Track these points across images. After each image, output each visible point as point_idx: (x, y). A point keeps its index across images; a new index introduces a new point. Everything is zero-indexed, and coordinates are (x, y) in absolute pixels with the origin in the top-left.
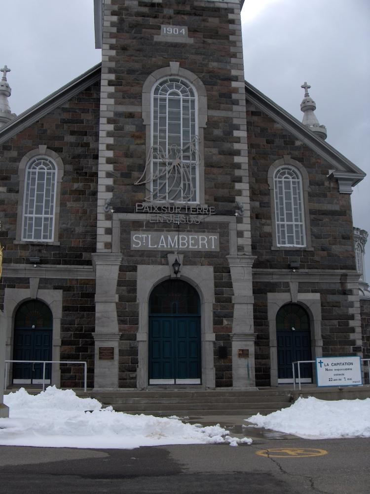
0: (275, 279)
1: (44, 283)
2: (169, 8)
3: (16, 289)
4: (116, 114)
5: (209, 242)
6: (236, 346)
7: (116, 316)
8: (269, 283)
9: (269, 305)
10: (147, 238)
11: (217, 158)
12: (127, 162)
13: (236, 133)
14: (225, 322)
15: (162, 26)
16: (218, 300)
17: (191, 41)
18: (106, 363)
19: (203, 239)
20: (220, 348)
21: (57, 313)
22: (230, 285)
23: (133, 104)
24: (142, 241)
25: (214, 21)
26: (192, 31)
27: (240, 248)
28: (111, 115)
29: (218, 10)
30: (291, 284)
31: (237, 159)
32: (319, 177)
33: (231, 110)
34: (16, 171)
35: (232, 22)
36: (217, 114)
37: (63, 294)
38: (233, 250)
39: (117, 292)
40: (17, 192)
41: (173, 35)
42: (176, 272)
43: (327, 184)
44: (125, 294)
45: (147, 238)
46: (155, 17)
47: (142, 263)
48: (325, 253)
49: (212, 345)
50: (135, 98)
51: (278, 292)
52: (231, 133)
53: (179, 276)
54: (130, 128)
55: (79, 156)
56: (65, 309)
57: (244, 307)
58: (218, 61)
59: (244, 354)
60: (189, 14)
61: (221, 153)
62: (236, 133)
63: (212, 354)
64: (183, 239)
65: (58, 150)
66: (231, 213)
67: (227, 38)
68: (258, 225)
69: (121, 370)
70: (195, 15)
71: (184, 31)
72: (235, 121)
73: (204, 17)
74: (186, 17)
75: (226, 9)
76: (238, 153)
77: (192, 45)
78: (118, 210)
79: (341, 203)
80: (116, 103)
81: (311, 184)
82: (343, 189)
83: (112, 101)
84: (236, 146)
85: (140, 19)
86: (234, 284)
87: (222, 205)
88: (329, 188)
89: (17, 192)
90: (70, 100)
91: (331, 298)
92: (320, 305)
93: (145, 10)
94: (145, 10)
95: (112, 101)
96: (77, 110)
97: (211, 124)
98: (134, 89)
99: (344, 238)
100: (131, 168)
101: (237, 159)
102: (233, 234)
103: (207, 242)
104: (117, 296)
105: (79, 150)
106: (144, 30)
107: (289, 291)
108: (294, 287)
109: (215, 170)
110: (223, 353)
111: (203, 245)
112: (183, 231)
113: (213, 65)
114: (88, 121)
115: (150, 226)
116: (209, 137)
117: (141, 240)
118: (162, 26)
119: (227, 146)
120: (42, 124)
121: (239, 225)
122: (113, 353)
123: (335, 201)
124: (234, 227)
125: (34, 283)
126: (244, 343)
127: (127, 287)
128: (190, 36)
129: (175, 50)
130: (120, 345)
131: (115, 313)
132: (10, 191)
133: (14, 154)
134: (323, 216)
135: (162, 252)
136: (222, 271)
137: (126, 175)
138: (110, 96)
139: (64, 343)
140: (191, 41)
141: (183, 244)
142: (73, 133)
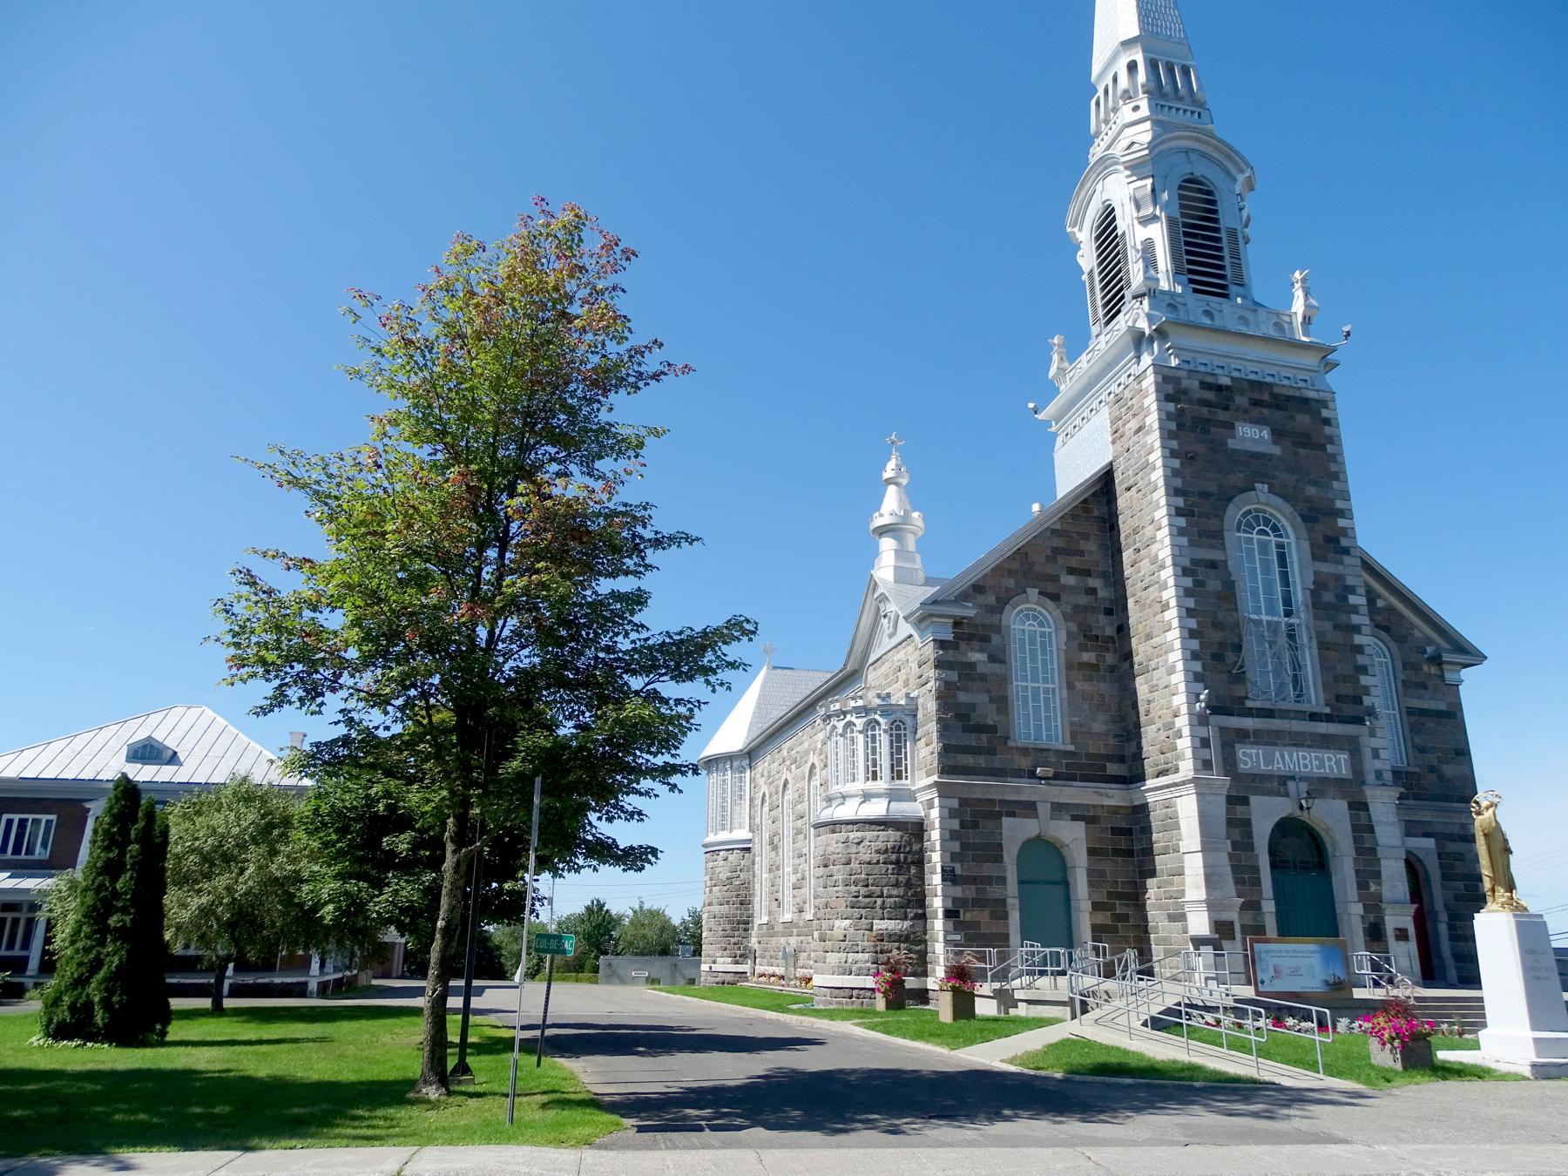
1: (1058, 809)
4: (1194, 562)
5: (1338, 763)
11: (1333, 636)
13: (1353, 600)
14: (1373, 888)
17: (1276, 450)
19: (1330, 759)
22: (1371, 829)
23: (1213, 547)
25: (1303, 420)
26: (1278, 435)
32: (1414, 658)
34: (998, 629)
35: (1327, 422)
36: (1325, 568)
38: (1370, 777)
41: (1254, 440)
43: (1425, 668)
46: (1226, 408)
49: (1359, 921)
50: (1214, 537)
52: (1345, 599)
53: (1305, 817)
54: (1214, 585)
55: (1086, 608)
56: (1092, 852)
57: (1393, 863)
58: (1315, 483)
60: (1269, 406)
61: (1337, 627)
62: (1353, 600)
63: (1361, 935)
64: (1304, 758)
65: (1055, 597)
66: (1360, 721)
67: (1323, 448)
70: (1278, 408)
71: (1266, 434)
72: (1350, 581)
74: (1266, 411)
80: (1192, 543)
84: (1355, 619)
85: (1205, 410)
86: (1377, 829)
87: (1348, 710)
91: (1453, 847)
93: (1210, 395)
94: (1210, 395)
102: (1367, 753)
103: (1334, 763)
105: (1084, 600)
109: (1331, 654)
113: (1311, 491)
115: (1259, 738)
117: (1251, 758)
119: (1342, 618)
124: (1368, 743)
125: (1044, 810)
128: (1275, 443)
131: (1229, 869)
132: (993, 659)
135: (1279, 777)
136: (1359, 807)
139: (1097, 907)
140: (1276, 450)
141: (1306, 766)
142: (1071, 571)
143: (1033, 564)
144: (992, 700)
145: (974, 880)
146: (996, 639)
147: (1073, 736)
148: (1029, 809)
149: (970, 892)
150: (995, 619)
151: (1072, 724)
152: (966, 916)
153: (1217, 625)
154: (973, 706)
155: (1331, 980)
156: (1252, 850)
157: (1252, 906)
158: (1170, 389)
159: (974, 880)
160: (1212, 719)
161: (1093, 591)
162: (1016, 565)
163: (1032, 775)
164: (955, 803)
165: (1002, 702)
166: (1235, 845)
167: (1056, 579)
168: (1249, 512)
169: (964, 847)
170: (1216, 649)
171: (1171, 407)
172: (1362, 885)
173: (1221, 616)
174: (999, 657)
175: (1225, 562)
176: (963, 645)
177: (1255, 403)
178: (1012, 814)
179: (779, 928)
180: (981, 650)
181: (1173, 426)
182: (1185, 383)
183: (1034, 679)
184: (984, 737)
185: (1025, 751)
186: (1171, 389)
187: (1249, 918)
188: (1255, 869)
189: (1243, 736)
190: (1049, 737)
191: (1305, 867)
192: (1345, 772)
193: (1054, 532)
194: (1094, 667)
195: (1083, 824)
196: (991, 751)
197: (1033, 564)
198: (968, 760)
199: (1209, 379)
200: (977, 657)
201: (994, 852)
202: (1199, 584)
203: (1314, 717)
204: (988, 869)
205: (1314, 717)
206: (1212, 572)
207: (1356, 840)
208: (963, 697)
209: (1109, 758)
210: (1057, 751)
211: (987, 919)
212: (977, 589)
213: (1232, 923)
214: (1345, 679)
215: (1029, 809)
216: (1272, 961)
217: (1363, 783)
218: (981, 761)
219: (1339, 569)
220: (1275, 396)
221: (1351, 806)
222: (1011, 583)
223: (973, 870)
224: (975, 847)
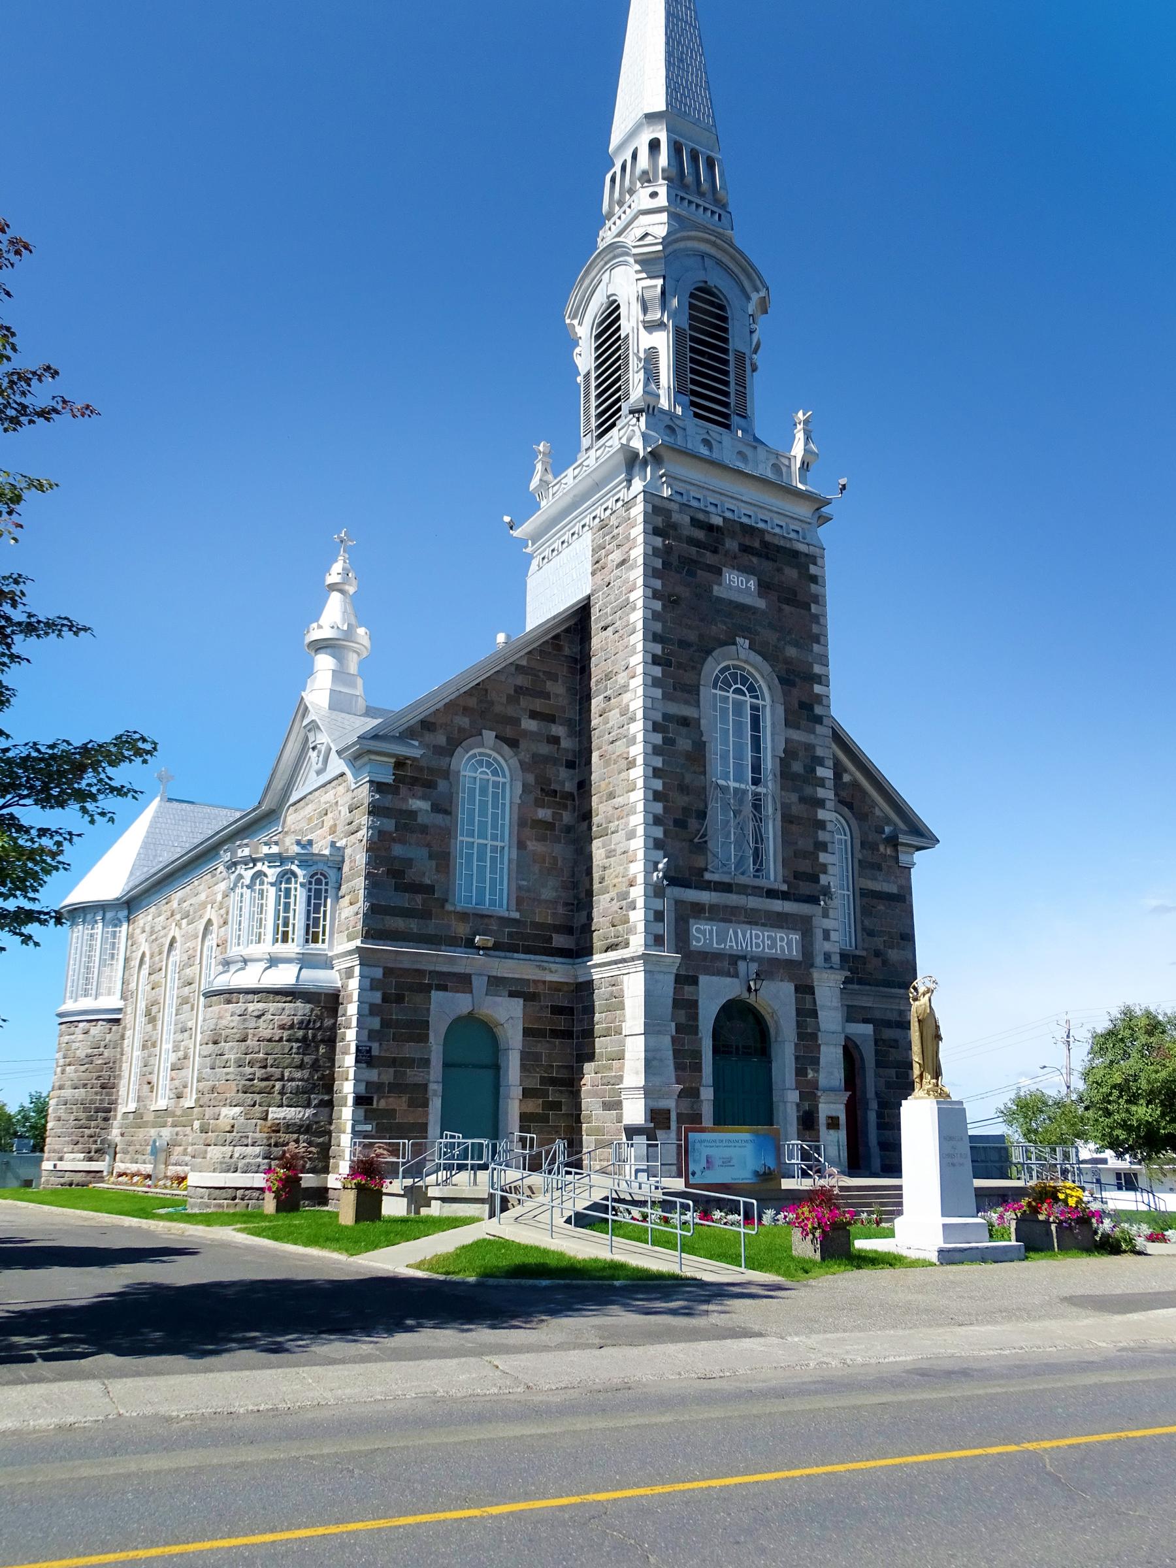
4: (666, 716)
5: (789, 944)
7: (671, 1057)
10: (711, 932)
11: (797, 809)
12: (682, 800)
14: (811, 1075)
17: (761, 604)
20: (805, 1112)
21: (513, 1038)
23: (687, 702)
24: (705, 936)
25: (791, 573)
26: (764, 587)
27: (827, 957)
29: (796, 554)
34: (446, 774)
38: (819, 960)
41: (739, 590)
43: (882, 848)
44: (683, 1020)
45: (711, 932)
49: (794, 1107)
50: (689, 692)
52: (814, 771)
56: (527, 1032)
57: (832, 1049)
58: (796, 644)
59: (833, 1123)
60: (757, 554)
64: (757, 937)
65: (513, 743)
66: (813, 900)
71: (752, 584)
72: (820, 752)
75: (807, 555)
80: (666, 697)
82: (903, 858)
87: (805, 888)
90: (529, 653)
91: (888, 1033)
92: (873, 1043)
93: (700, 535)
94: (700, 535)
96: (541, 674)
97: (790, 753)
98: (688, 677)
99: (902, 939)
100: (686, 810)
102: (819, 934)
103: (786, 944)
104: (673, 1024)
105: (545, 749)
106: (699, 572)
111: (782, 947)
112: (756, 924)
113: (791, 652)
114: (557, 695)
117: (704, 934)
119: (808, 790)
121: (825, 920)
122: (669, 1119)
125: (479, 984)
126: (832, 1106)
128: (760, 595)
130: (677, 1106)
132: (437, 808)
134: (875, 901)
135: (731, 956)
136: (805, 990)
140: (761, 604)
142: (534, 715)
143: (492, 703)
144: (431, 857)
145: (393, 1062)
146: (442, 785)
147: (519, 901)
148: (463, 982)
149: (388, 1076)
151: (519, 888)
153: (683, 789)
154: (409, 862)
155: (761, 1170)
156: (697, 1034)
158: (659, 521)
159: (393, 1062)
160: (669, 891)
161: (555, 740)
162: (472, 702)
163: (470, 944)
164: (378, 973)
165: (443, 859)
166: (679, 1028)
167: (516, 722)
169: (385, 1024)
172: (800, 1072)
173: (688, 778)
174: (444, 808)
176: (403, 790)
177: (745, 549)
178: (444, 988)
179: (149, 1117)
180: (424, 798)
181: (658, 563)
183: (482, 835)
184: (419, 898)
185: (464, 916)
188: (697, 1054)
189: (698, 910)
190: (492, 902)
192: (795, 953)
193: (519, 668)
194: (550, 826)
195: (521, 1001)
196: (424, 914)
197: (492, 703)
198: (399, 923)
200: (418, 804)
201: (418, 1030)
204: (409, 1050)
206: (684, 730)
207: (799, 1025)
208: (398, 850)
209: (558, 929)
211: (404, 1107)
212: (427, 725)
213: (669, 1111)
215: (463, 982)
217: (812, 965)
218: (413, 925)
220: (766, 544)
221: (797, 989)
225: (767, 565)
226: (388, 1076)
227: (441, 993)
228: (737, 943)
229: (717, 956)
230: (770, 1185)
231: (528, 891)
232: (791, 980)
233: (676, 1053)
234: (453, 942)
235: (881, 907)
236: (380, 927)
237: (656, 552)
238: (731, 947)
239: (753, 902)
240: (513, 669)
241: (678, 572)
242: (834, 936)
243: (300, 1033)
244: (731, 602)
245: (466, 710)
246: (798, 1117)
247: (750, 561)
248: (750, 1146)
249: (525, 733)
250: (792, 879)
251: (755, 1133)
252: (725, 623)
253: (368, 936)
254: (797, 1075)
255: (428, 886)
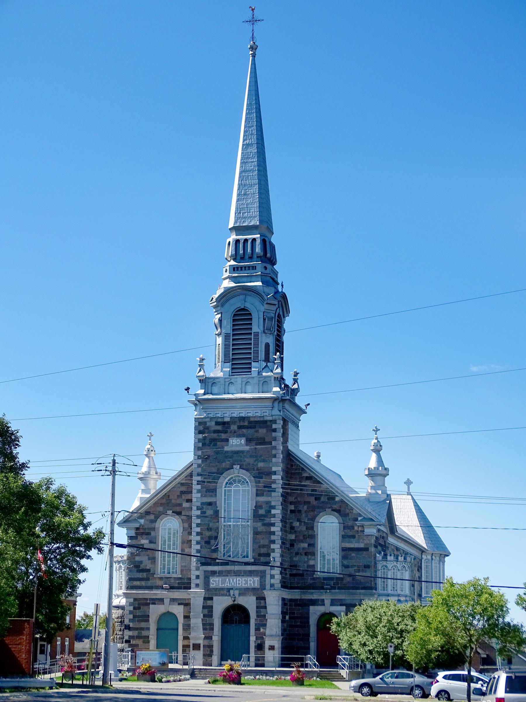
0: (315, 597)
2: (235, 424)
3: (156, 606)
4: (202, 504)
5: (254, 582)
6: (268, 643)
8: (311, 599)
9: (310, 614)
10: (219, 581)
14: (262, 630)
15: (230, 439)
16: (258, 616)
17: (247, 448)
18: (196, 652)
20: (258, 644)
22: (265, 607)
23: (212, 496)
25: (262, 431)
26: (249, 441)
27: (272, 585)
28: (199, 504)
29: (265, 422)
30: (325, 601)
31: (273, 529)
33: (271, 496)
34: (154, 529)
37: (184, 608)
38: (268, 586)
39: (202, 612)
40: (155, 543)
41: (237, 445)
42: (234, 601)
45: (219, 581)
46: (226, 432)
47: (216, 595)
48: (351, 578)
50: (213, 492)
51: (317, 605)
52: (270, 511)
53: (236, 603)
54: (210, 512)
57: (273, 620)
58: (264, 461)
59: (272, 648)
61: (264, 525)
62: (273, 512)
65: (179, 513)
68: (306, 559)
69: (204, 655)
70: (251, 428)
71: (243, 441)
72: (273, 504)
73: (257, 429)
74: (245, 431)
75: (271, 421)
76: (273, 525)
77: (248, 451)
78: (203, 564)
79: (365, 542)
81: (344, 528)
83: (199, 495)
86: (268, 607)
87: (263, 559)
88: (358, 531)
89: (155, 543)
93: (219, 428)
94: (219, 428)
95: (199, 495)
97: (258, 507)
100: (210, 538)
101: (273, 529)
102: (268, 577)
103: (253, 582)
107: (324, 605)
108: (327, 602)
110: (260, 647)
111: (250, 584)
112: (239, 576)
113: (261, 465)
115: (221, 573)
116: (257, 516)
117: (215, 582)
118: (230, 439)
119: (267, 520)
120: (169, 496)
122: (200, 647)
123: (361, 540)
127: (208, 611)
129: (236, 457)
132: (151, 542)
133: (152, 517)
134: (350, 552)
135: (227, 589)
136: (261, 599)
137: (208, 543)
138: (199, 491)
140: (247, 448)
143: (171, 500)
144: (149, 559)
145: (137, 629)
146: (153, 533)
147: (182, 571)
149: (136, 633)
150: (152, 525)
151: (182, 566)
152: (133, 642)
153: (209, 529)
154: (141, 562)
155: (162, 662)
156: (212, 617)
157: (208, 638)
158: (201, 428)
159: (137, 629)
160: (201, 568)
162: (164, 501)
163: (162, 588)
164: (132, 600)
167: (180, 505)
168: (232, 478)
170: (207, 539)
171: (201, 436)
172: (257, 629)
173: (211, 525)
175: (216, 503)
176: (139, 537)
177: (240, 427)
178: (154, 604)
180: (146, 539)
181: (200, 445)
182: (208, 424)
184: (145, 574)
185: (161, 579)
186: (201, 427)
187: (207, 642)
188: (212, 625)
189: (214, 573)
191: (241, 622)
192: (257, 585)
193: (182, 484)
195: (183, 606)
196: (147, 579)
197: (171, 500)
198: (137, 583)
199: (220, 420)
201: (146, 618)
202: (203, 513)
203: (246, 564)
204: (143, 625)
205: (246, 564)
206: (210, 507)
207: (257, 612)
208: (137, 558)
210: (174, 578)
211: (142, 643)
212: (147, 513)
213: (200, 644)
214: (264, 546)
216: (142, 657)
217: (265, 589)
218: (143, 583)
219: (269, 499)
220: (250, 422)
221: (257, 599)
222: (161, 509)
223: (137, 625)
224: (139, 617)
225: (251, 431)
226: (136, 633)
227: (153, 606)
228: (230, 584)
229: (222, 589)
230: (165, 667)
231: (185, 567)
232: (254, 595)
233: (204, 625)
234: (157, 587)
235: (353, 555)
236: (132, 585)
237: (199, 440)
238: (227, 585)
239: (237, 568)
240: (179, 485)
241: (209, 446)
242: (276, 577)
243: (120, 620)
244: (232, 451)
245: (162, 504)
246: (255, 646)
247: (243, 432)
248: (158, 655)
249: (184, 508)
250: (257, 557)
251: (160, 651)
252: (229, 461)
253: (128, 588)
254: (256, 630)
255: (148, 569)
